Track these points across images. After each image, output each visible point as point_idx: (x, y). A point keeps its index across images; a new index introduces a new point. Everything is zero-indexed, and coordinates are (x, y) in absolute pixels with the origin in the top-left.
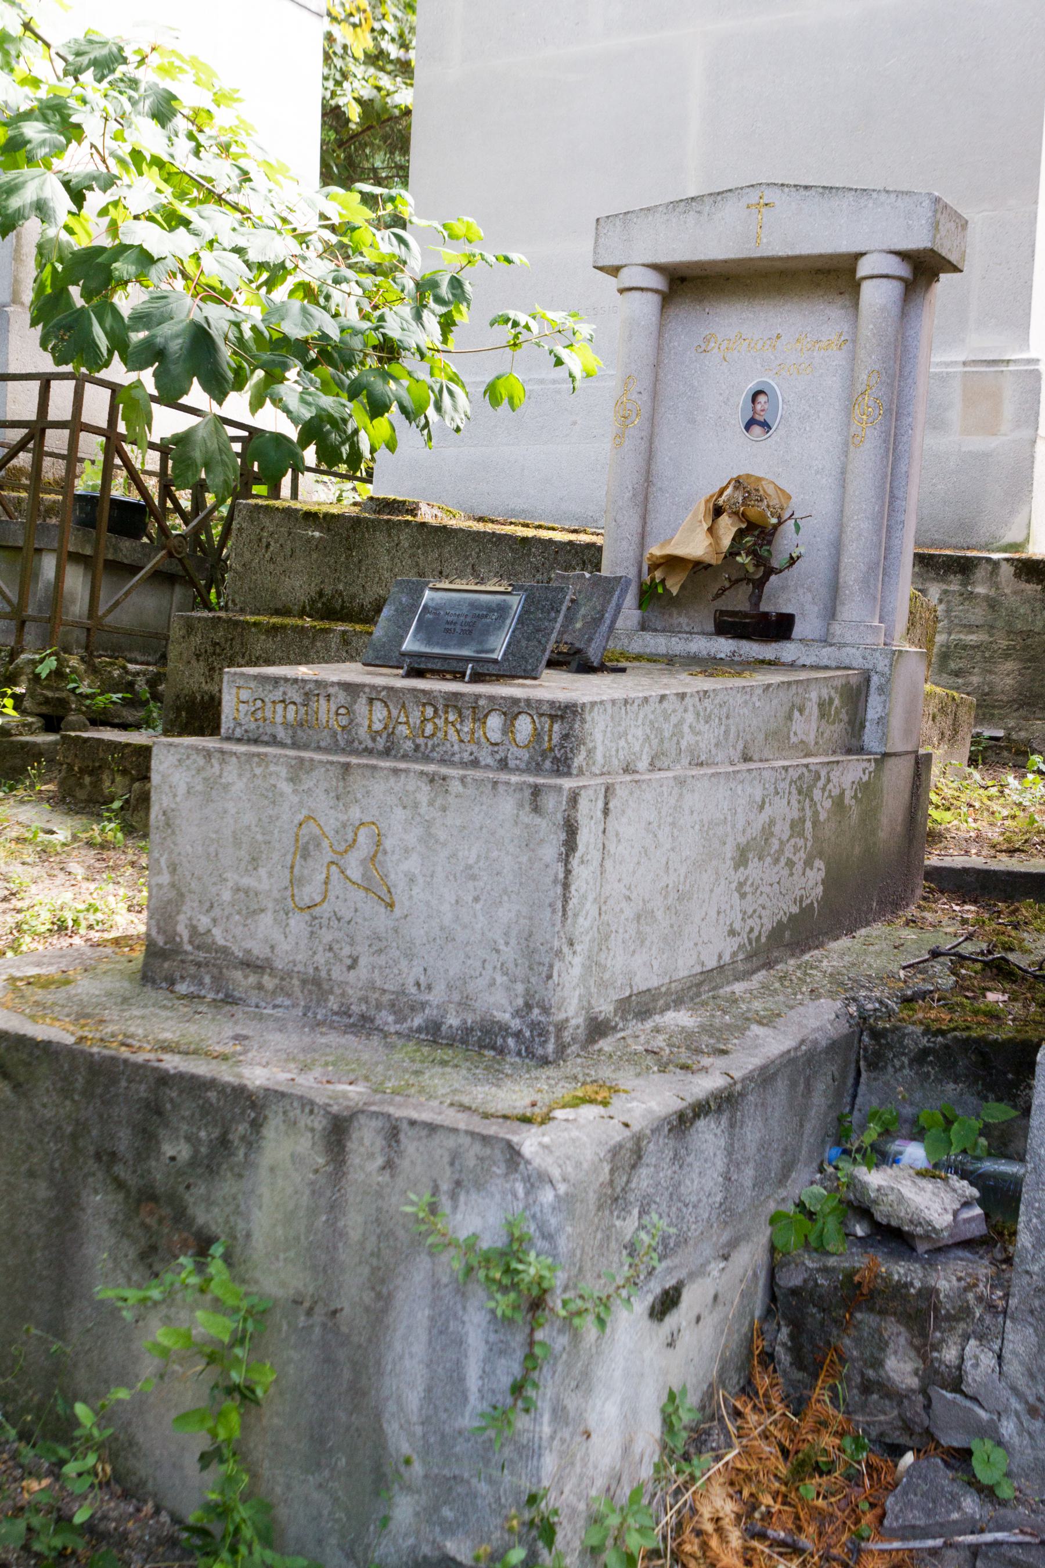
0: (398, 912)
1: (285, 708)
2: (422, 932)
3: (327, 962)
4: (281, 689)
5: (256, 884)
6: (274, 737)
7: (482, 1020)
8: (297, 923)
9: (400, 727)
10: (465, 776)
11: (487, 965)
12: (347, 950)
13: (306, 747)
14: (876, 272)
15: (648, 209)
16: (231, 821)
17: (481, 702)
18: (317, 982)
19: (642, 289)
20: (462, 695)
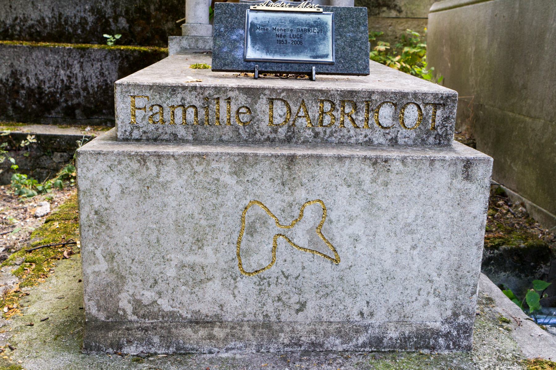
0: (343, 264)
1: (185, 112)
2: (365, 276)
3: (276, 310)
4: (179, 96)
5: (202, 260)
6: (175, 135)
7: (417, 330)
8: (246, 286)
9: (300, 120)
10: (405, 158)
11: (421, 292)
12: (295, 298)
13: (208, 142)
16: (173, 213)
17: (374, 97)
18: (267, 326)
20: (357, 92)
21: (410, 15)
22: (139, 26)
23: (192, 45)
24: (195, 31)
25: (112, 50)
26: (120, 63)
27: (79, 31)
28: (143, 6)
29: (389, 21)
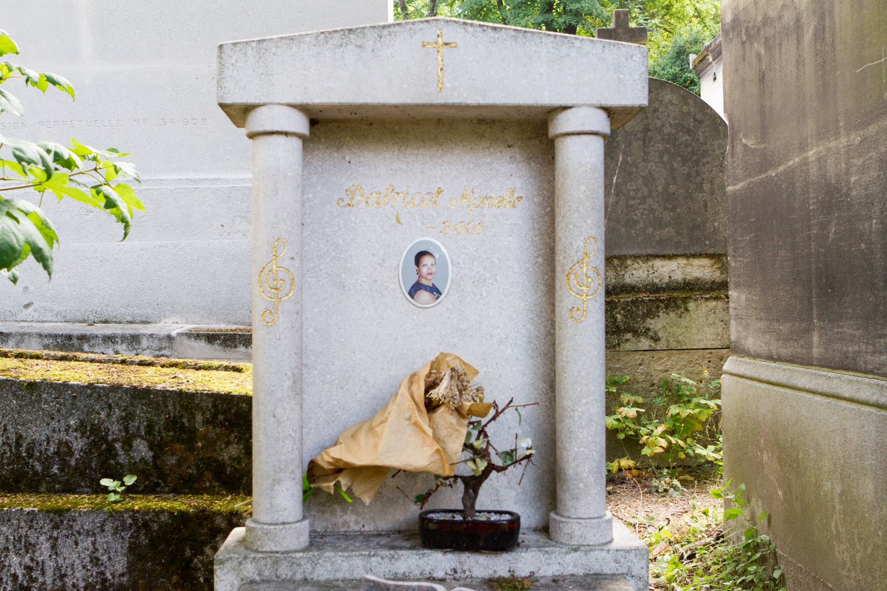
14: (586, 128)
15: (291, 39)
19: (286, 134)
21: (673, 345)
22: (173, 455)
23: (267, 573)
24: (272, 540)
25: (117, 512)
26: (132, 537)
27: (55, 469)
28: (182, 416)
29: (637, 357)
